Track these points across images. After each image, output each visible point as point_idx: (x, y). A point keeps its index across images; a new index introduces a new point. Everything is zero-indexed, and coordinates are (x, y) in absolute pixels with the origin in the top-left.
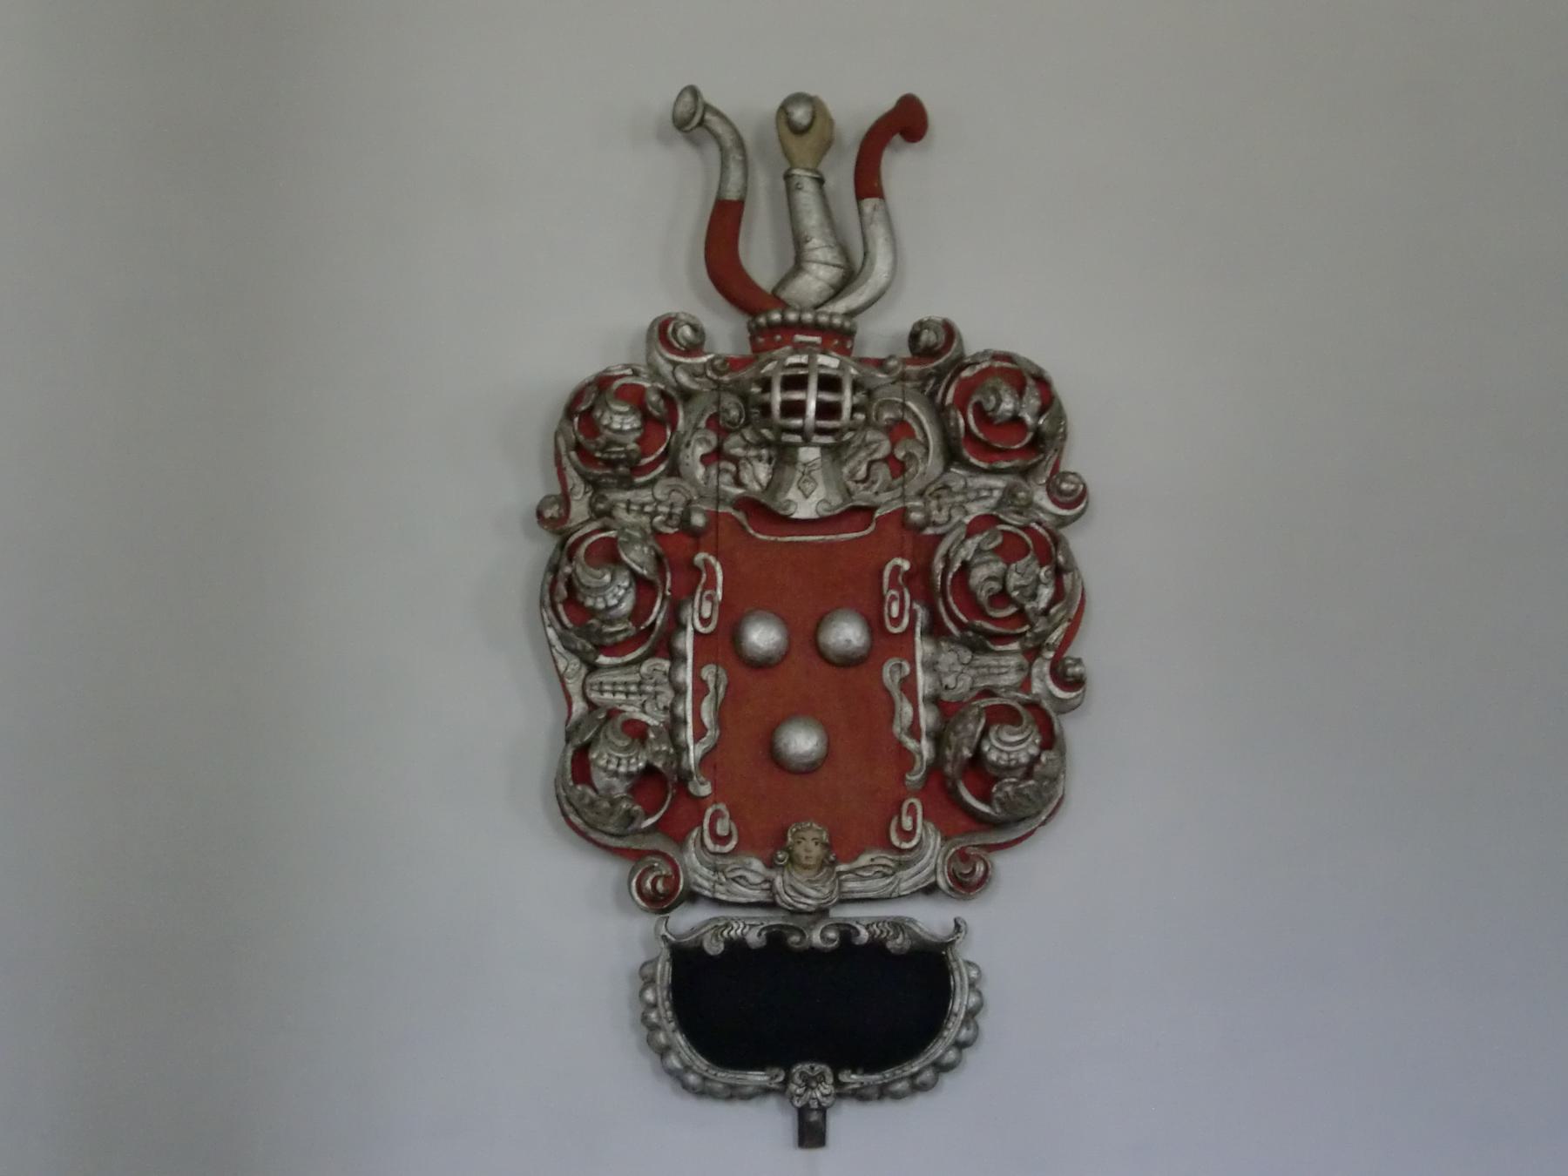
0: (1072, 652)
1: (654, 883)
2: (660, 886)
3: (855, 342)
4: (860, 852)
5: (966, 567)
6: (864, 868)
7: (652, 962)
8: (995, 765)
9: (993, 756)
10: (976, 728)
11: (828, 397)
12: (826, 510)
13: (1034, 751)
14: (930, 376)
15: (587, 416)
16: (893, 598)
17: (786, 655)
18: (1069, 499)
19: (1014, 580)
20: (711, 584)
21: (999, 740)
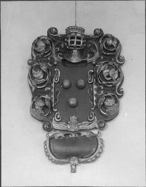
0: (122, 87)
1: (46, 126)
2: (47, 127)
5: (102, 71)
6: (84, 124)
7: (46, 141)
8: (107, 106)
10: (103, 99)
13: (113, 103)
14: (98, 38)
15: (36, 44)
16: (90, 77)
17: (77, 100)
18: (121, 60)
19: (110, 74)
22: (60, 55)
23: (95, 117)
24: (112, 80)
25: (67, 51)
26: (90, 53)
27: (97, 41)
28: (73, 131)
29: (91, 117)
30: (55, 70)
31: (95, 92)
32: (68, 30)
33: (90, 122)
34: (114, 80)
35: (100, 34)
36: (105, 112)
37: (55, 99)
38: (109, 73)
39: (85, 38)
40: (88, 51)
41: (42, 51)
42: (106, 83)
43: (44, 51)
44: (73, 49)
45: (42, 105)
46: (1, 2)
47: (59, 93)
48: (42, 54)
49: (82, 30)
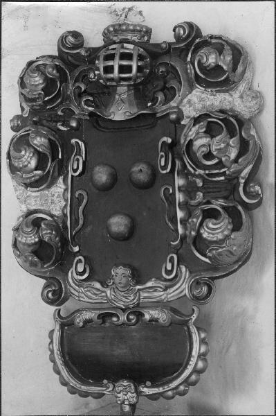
2: (50, 295)
3: (152, 36)
4: (149, 280)
5: (191, 142)
9: (205, 235)
11: (125, 63)
12: (128, 116)
13: (226, 233)
16: (162, 156)
19: (214, 148)
20: (79, 153)
21: (208, 228)
22: (87, 103)
23: (184, 269)
24: (220, 164)
25: (103, 93)
26: (163, 89)
27: (182, 56)
28: (123, 307)
29: (169, 268)
30: (73, 141)
31: (180, 197)
32: (106, 34)
33: (168, 284)
34: (228, 164)
35: (189, 36)
36: (205, 255)
37: (73, 218)
38: (210, 146)
39: (145, 53)
40: (157, 86)
41: (37, 96)
42: (207, 172)
43: (42, 96)
44: (116, 86)
45: (33, 241)
46: (273, 3)
47: (85, 201)
48: (40, 102)
49: (140, 31)
